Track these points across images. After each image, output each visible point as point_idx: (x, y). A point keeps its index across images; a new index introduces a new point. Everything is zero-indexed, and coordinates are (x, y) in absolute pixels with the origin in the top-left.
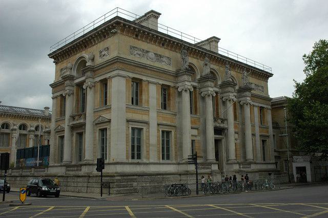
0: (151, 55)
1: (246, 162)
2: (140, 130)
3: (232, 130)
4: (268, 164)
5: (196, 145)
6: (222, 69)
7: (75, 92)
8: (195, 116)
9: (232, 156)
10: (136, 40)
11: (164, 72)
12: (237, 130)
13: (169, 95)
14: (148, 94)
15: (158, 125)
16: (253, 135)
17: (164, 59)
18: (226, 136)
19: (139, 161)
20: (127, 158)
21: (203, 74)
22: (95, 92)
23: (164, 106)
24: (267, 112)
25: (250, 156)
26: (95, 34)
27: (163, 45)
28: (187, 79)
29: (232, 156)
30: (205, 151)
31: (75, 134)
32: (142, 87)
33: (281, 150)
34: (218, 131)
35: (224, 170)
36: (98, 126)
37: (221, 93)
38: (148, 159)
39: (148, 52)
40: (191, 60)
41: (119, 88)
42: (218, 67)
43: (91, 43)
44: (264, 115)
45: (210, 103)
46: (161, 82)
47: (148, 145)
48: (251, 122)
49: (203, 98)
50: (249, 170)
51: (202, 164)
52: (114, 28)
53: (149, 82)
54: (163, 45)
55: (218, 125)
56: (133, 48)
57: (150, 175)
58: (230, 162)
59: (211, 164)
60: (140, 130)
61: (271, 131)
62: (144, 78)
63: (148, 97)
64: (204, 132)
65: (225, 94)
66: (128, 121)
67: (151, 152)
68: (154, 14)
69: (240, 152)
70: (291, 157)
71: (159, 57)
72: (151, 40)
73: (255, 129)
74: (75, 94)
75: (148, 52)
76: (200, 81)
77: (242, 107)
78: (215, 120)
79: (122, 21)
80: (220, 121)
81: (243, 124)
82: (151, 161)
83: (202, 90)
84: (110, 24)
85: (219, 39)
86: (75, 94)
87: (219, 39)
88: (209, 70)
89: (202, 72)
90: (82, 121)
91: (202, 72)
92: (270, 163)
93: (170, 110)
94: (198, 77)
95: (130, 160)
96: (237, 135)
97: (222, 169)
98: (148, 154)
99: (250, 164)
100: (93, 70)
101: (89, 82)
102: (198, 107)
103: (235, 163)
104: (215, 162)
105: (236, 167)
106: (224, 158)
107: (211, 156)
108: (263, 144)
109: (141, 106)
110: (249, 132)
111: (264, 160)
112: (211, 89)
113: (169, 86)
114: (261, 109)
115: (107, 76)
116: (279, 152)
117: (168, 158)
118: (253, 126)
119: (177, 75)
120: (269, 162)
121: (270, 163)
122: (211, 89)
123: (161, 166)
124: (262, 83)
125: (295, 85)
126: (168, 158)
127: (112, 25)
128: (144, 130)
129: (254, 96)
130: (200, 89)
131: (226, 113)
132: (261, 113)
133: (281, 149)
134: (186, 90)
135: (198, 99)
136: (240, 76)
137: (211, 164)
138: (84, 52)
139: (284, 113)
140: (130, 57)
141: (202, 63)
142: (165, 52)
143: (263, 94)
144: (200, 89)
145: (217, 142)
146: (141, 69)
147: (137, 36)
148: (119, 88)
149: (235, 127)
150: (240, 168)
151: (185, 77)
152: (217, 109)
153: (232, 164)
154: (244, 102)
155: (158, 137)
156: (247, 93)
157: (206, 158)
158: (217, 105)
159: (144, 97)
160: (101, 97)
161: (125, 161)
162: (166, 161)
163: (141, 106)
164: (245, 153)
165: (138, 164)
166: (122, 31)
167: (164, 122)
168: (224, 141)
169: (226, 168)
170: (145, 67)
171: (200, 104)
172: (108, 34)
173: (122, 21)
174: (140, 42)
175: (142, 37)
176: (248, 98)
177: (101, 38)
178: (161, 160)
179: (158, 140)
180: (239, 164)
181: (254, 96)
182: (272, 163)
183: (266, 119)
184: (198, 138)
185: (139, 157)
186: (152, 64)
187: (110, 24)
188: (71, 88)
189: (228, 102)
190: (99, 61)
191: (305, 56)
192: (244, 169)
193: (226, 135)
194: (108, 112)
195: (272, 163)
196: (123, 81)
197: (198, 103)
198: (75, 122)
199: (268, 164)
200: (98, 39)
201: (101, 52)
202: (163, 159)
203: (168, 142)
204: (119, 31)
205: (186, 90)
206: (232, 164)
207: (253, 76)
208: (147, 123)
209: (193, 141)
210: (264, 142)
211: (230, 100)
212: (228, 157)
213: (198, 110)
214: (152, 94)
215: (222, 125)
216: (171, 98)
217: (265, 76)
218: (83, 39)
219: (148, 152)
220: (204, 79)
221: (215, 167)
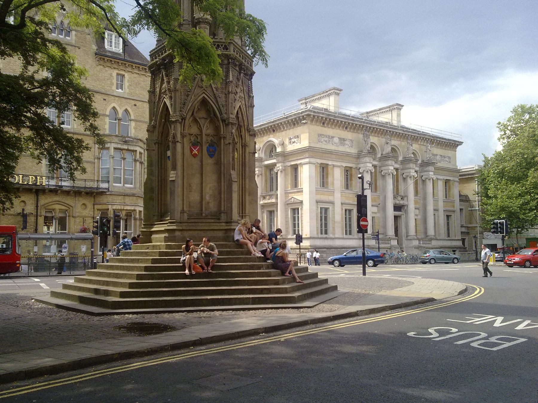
0: (336, 140)
1: (427, 238)
2: (326, 209)
3: (412, 206)
4: (453, 240)
5: (376, 221)
6: (403, 143)
7: (263, 172)
8: (375, 194)
9: (412, 232)
10: (322, 128)
11: (348, 155)
12: (417, 206)
13: (351, 175)
14: (333, 177)
15: (342, 204)
16: (436, 210)
17: (347, 142)
18: (406, 212)
19: (326, 236)
20: (317, 234)
21: (384, 153)
22: (286, 175)
23: (347, 187)
24: (453, 184)
25: (431, 232)
26: (285, 122)
27: (346, 128)
28: (368, 161)
29: (412, 232)
30: (385, 227)
31: (265, 212)
32: (328, 171)
33: (470, 225)
34: (397, 208)
35: (404, 246)
36: (289, 205)
37: (402, 169)
38: (334, 234)
39: (333, 137)
40: (374, 139)
41: (307, 173)
42: (399, 142)
43: (280, 128)
44: (449, 187)
45: (390, 181)
46: (344, 165)
47: (334, 222)
48: (433, 197)
49: (384, 176)
50: (430, 246)
51: (383, 240)
52: (304, 119)
53: (334, 166)
54: (346, 128)
55: (398, 202)
56: (320, 135)
57: (336, 248)
58: (409, 238)
59: (390, 239)
60: (326, 209)
61: (458, 205)
62: (330, 163)
63: (333, 180)
64: (384, 209)
65: (406, 171)
66: (317, 202)
67: (336, 229)
68: (336, 91)
69: (421, 228)
70: (482, 233)
71: (342, 140)
72: (336, 126)
73: (438, 204)
74: (263, 174)
75: (333, 137)
76: (380, 159)
77: (424, 181)
78: (395, 197)
79: (312, 113)
80: (399, 198)
81: (425, 198)
82: (337, 236)
83: (383, 168)
84: (301, 115)
85: (402, 106)
86: (263, 174)
87: (402, 106)
88: (390, 149)
89: (383, 150)
90: (274, 200)
91: (383, 150)
92: (455, 240)
93: (351, 190)
94: (379, 155)
95: (320, 236)
96: (417, 211)
97: (402, 245)
98: (334, 230)
99: (431, 240)
100: (285, 156)
101: (279, 166)
102: (378, 184)
103: (414, 239)
104: (394, 237)
105: (416, 243)
106: (403, 233)
107: (391, 232)
108: (448, 219)
109: (327, 188)
110: (430, 208)
111: (449, 236)
112: (391, 167)
113: (351, 168)
114: (447, 182)
115: (298, 162)
116: (468, 227)
117: (350, 234)
118: (436, 201)
119: (359, 156)
120: (454, 238)
121: (455, 240)
122: (391, 167)
123: (345, 241)
124: (449, 153)
125: (484, 159)
126: (350, 234)
127: (303, 116)
128: (330, 209)
129: (438, 170)
130: (380, 167)
131: (406, 190)
132: (446, 186)
133: (471, 224)
134: (367, 172)
135: (378, 178)
136: (424, 148)
137: (390, 239)
138: (271, 136)
139: (472, 189)
140: (318, 145)
141: (383, 140)
142: (348, 135)
143: (450, 166)
144: (380, 167)
145: (396, 218)
146: (327, 155)
147: (323, 124)
148: (307, 173)
149: (416, 202)
150: (419, 243)
151: (367, 159)
152: (397, 186)
153: (411, 240)
154: (427, 177)
155: (342, 215)
156: (431, 168)
157: (385, 234)
158: (397, 181)
159: (330, 180)
160: (291, 180)
161: (316, 236)
162: (348, 236)
163: (327, 188)
164: (426, 229)
165: (326, 238)
166: (312, 121)
167: (347, 202)
168: (403, 217)
169: (405, 243)
170: (330, 152)
171: (380, 182)
172: (298, 123)
173: (312, 113)
174: (326, 129)
175: (328, 124)
176: (431, 173)
177: (290, 125)
178: (345, 235)
179: (342, 218)
180: (419, 240)
181: (438, 170)
182: (458, 240)
183: (451, 192)
184: (378, 215)
185: (326, 233)
186: (336, 148)
187: (301, 115)
188: (260, 169)
189: (408, 178)
190: (290, 148)
191: (499, 123)
192: (424, 245)
193: (405, 211)
194: (300, 194)
195: (458, 240)
196: (313, 167)
197: (378, 181)
198: (266, 201)
199: (453, 240)
200: (287, 127)
201: (290, 139)
202: (321, 234)
203: (350, 219)
204: (309, 122)
205: (367, 172)
206: (411, 240)
207: (439, 147)
208: (332, 203)
209: (373, 217)
210: (448, 217)
211: (411, 177)
212: (407, 232)
213: (378, 189)
214: (337, 176)
215: (402, 202)
216: (353, 179)
217: (453, 145)
218: (272, 124)
219: (334, 228)
220: (385, 158)
221: (394, 243)
